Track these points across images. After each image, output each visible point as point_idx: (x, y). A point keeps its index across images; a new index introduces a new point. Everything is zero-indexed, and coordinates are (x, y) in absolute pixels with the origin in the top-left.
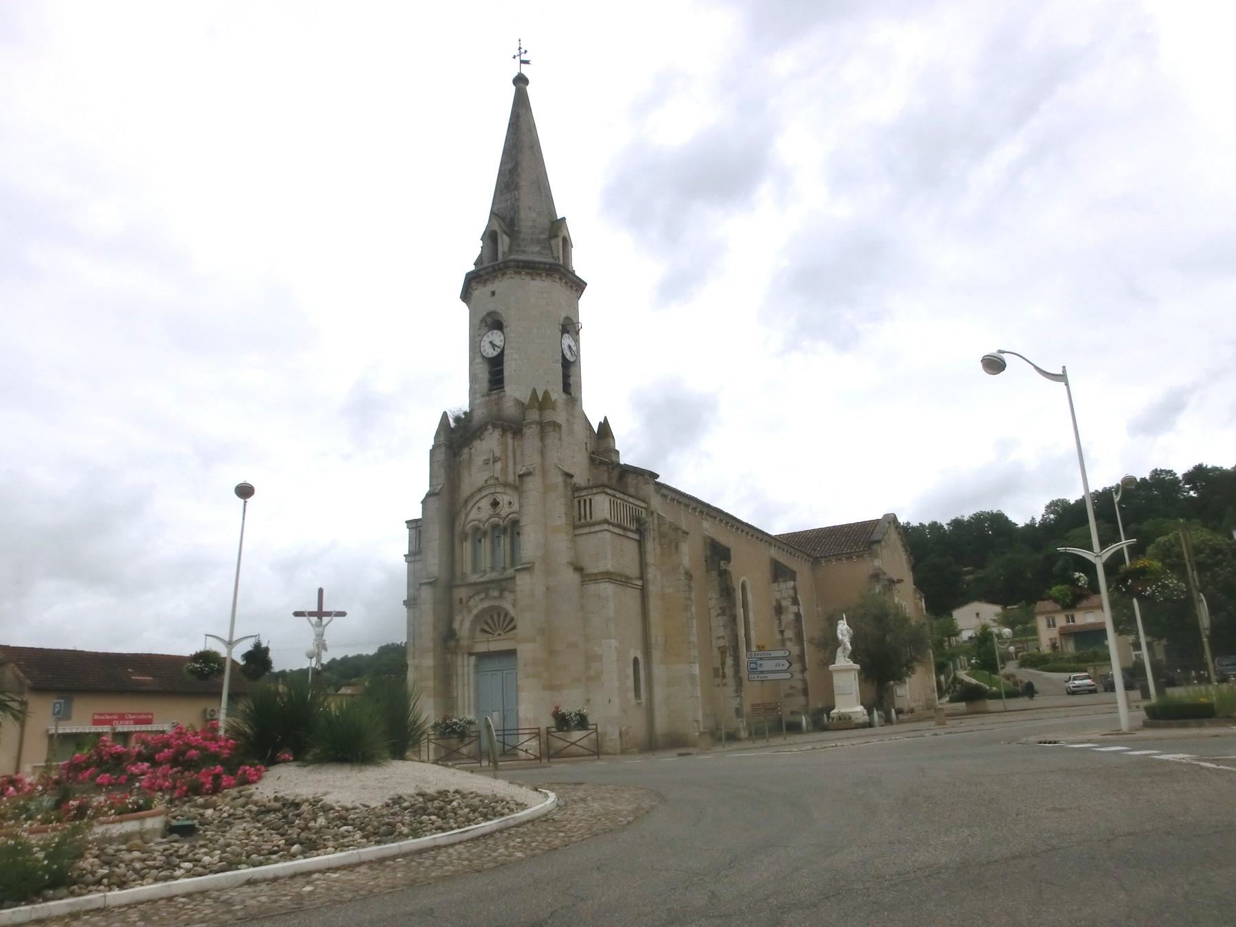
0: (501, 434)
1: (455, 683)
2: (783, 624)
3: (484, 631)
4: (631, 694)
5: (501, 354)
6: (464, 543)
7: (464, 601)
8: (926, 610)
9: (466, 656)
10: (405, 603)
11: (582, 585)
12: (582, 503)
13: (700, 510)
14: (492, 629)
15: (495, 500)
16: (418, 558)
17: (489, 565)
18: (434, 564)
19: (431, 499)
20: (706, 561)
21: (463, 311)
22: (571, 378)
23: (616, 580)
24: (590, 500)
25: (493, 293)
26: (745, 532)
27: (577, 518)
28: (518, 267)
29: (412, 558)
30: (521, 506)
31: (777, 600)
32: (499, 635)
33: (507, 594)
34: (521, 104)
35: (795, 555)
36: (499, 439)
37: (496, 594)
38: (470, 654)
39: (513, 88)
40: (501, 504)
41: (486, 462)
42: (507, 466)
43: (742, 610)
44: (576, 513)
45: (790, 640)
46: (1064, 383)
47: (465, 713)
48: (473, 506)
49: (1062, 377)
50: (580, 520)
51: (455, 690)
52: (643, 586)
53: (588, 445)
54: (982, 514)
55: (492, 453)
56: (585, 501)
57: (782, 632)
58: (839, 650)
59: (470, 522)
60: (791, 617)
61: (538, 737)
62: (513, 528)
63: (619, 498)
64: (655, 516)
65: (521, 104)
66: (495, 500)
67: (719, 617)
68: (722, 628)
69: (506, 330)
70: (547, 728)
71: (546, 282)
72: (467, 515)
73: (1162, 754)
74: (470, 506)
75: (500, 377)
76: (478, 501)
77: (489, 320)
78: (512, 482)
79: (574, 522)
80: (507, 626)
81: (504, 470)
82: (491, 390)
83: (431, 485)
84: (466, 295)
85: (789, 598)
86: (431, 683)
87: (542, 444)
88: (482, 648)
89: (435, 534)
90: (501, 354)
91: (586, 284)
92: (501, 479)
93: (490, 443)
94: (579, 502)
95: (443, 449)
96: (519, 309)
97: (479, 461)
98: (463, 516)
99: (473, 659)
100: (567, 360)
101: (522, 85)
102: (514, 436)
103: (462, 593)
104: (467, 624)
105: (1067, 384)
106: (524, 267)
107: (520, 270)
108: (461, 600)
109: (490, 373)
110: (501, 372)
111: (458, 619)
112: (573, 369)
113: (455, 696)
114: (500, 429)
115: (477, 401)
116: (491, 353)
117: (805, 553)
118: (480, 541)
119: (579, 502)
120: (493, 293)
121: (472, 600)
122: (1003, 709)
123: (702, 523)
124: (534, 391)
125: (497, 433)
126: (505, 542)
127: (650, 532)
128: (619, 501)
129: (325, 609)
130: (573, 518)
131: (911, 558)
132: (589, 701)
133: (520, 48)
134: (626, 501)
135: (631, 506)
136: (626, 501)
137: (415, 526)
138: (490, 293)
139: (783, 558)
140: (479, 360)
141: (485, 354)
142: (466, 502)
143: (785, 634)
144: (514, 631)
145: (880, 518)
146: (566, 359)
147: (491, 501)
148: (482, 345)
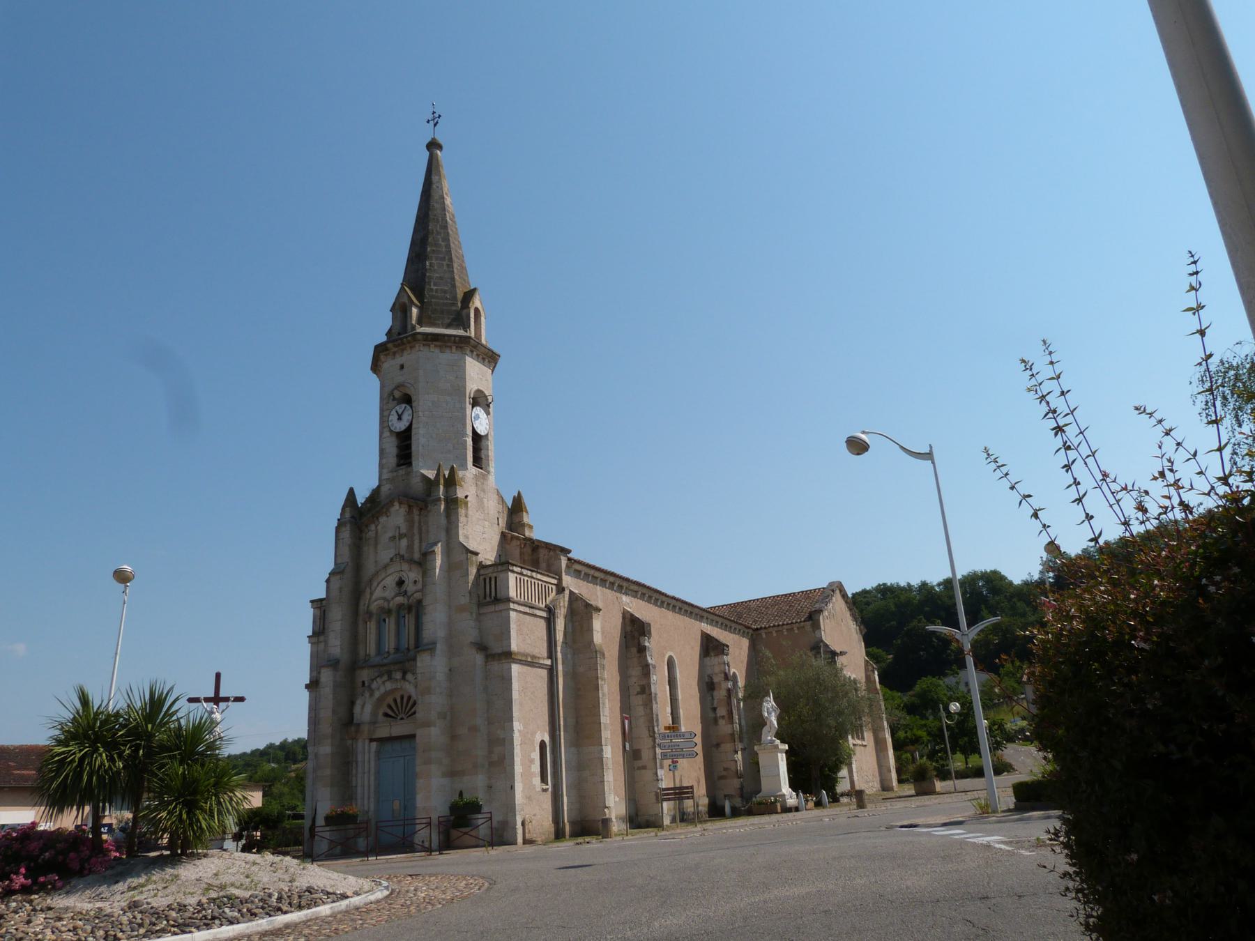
1: (354, 771)
2: (716, 701)
3: (386, 715)
4: (537, 780)
5: (409, 428)
6: (368, 623)
7: (366, 684)
8: (880, 683)
9: (367, 742)
10: (307, 686)
11: (486, 666)
12: (488, 581)
13: (619, 585)
14: (395, 713)
15: (400, 578)
16: (322, 638)
17: (392, 645)
18: (336, 645)
19: (336, 579)
20: (625, 637)
21: (374, 382)
22: (482, 451)
23: (520, 660)
24: (496, 578)
25: (402, 367)
26: (671, 606)
28: (426, 340)
29: (315, 640)
30: (424, 586)
31: (708, 676)
32: (402, 719)
33: (409, 676)
34: (432, 168)
35: (731, 627)
36: (405, 516)
37: (398, 675)
38: (371, 740)
42: (413, 544)
43: (668, 687)
44: (481, 593)
45: (723, 717)
46: (930, 461)
47: (364, 804)
49: (929, 456)
50: (485, 598)
51: (354, 778)
52: (552, 666)
53: (500, 519)
54: (975, 573)
56: (490, 579)
57: (714, 709)
58: (765, 730)
59: (376, 600)
60: (723, 693)
61: (429, 827)
62: (416, 609)
63: (526, 576)
64: (567, 592)
65: (432, 168)
66: (400, 578)
67: (639, 696)
68: (642, 707)
70: (439, 817)
72: (371, 594)
73: (986, 836)
74: (375, 584)
75: (407, 452)
76: (383, 579)
77: (397, 394)
80: (406, 709)
81: (410, 547)
82: (399, 465)
83: (336, 564)
84: (376, 367)
85: (721, 673)
86: (328, 772)
87: (448, 522)
88: (383, 732)
89: (338, 618)
90: (409, 428)
91: (499, 356)
93: (396, 518)
94: (485, 580)
96: (427, 382)
97: (384, 538)
98: (368, 596)
99: (374, 744)
100: (478, 434)
103: (364, 675)
104: (368, 709)
105: (933, 463)
108: (363, 682)
110: (409, 447)
111: (359, 703)
112: (483, 443)
113: (354, 784)
114: (406, 506)
115: (385, 476)
116: (401, 426)
117: (742, 625)
118: (384, 620)
119: (485, 580)
120: (402, 367)
121: (375, 682)
122: (953, 790)
123: (622, 598)
124: (351, 492)
126: (410, 621)
127: (560, 610)
128: (526, 578)
129: (222, 694)
130: (479, 597)
131: (862, 627)
132: (491, 787)
133: (434, 113)
135: (540, 583)
136: (534, 578)
137: (319, 606)
139: (715, 632)
140: (387, 434)
141: (392, 429)
142: (371, 581)
143: (718, 711)
144: (414, 716)
145: (825, 586)
146: (476, 431)
147: (397, 579)
148: (390, 419)
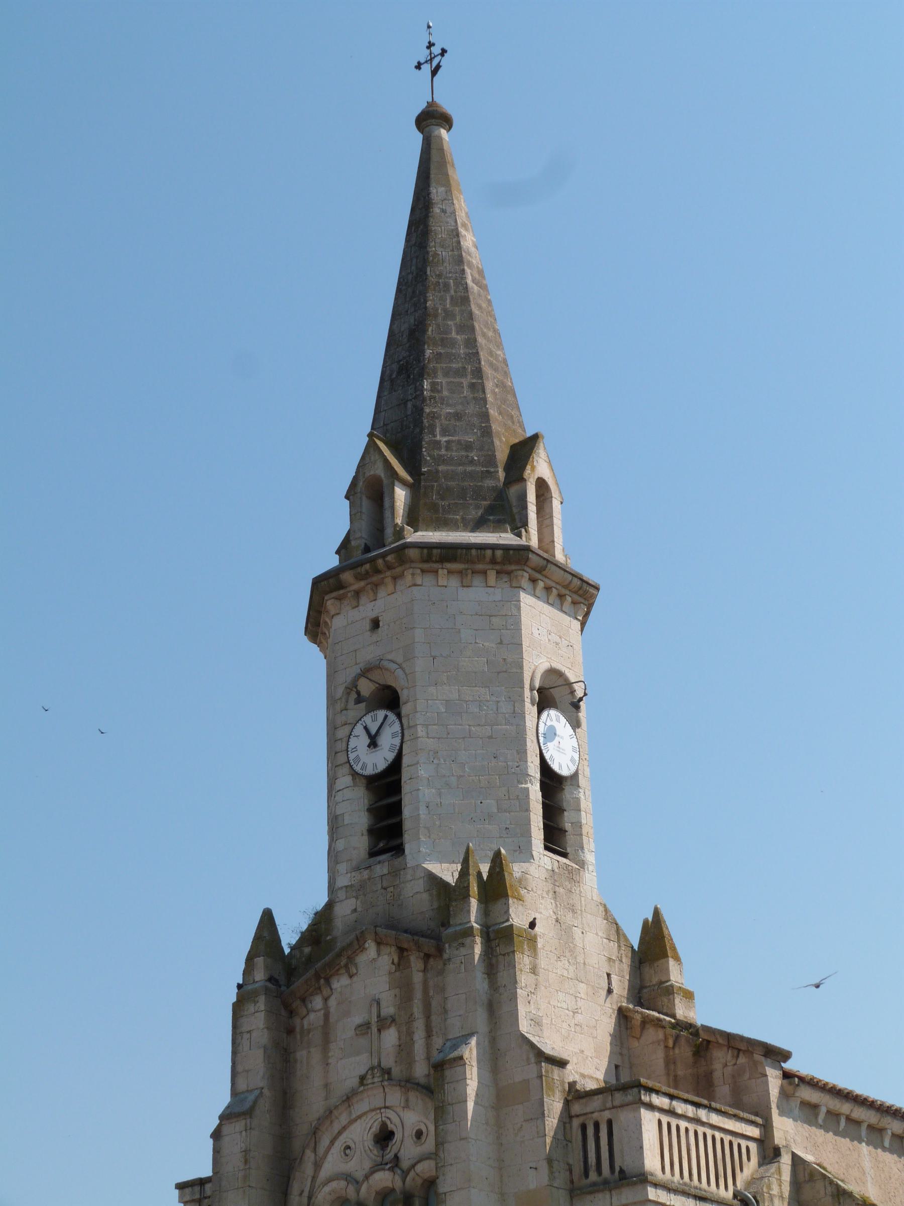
0: (396, 960)
5: (395, 766)
12: (590, 1131)
15: (384, 1125)
22: (566, 813)
25: (375, 624)
27: (578, 1168)
28: (428, 559)
39: (218, 1122)
40: (398, 1136)
41: (364, 1028)
48: (332, 1143)
50: (586, 1175)
53: (614, 978)
55: (374, 1010)
56: (597, 1125)
64: (786, 1160)
66: (384, 1125)
69: (405, 709)
71: (498, 591)
72: (318, 1166)
74: (325, 1141)
77: (366, 688)
78: (423, 1081)
79: (572, 1182)
81: (405, 1049)
90: (395, 766)
91: (597, 588)
92: (396, 1072)
94: (584, 1127)
95: (262, 1003)
98: (308, 1168)
101: (203, 1182)
102: (426, 964)
106: (443, 560)
107: (435, 566)
109: (372, 810)
110: (396, 809)
114: (393, 949)
115: (343, 881)
119: (584, 1127)
120: (375, 624)
125: (386, 960)
128: (683, 1124)
133: (430, 45)
134: (703, 1124)
135: (718, 1135)
136: (703, 1124)
138: (367, 625)
140: (345, 780)
141: (358, 768)
142: (315, 1132)
147: (376, 1128)
148: (351, 745)
